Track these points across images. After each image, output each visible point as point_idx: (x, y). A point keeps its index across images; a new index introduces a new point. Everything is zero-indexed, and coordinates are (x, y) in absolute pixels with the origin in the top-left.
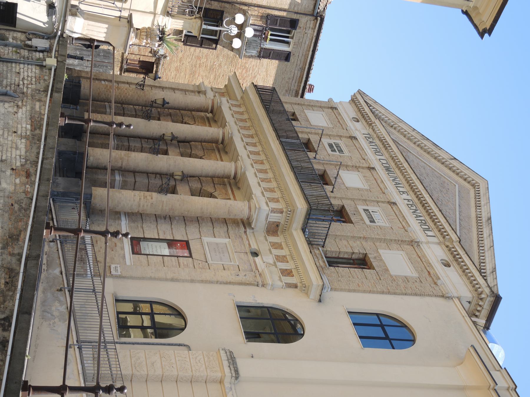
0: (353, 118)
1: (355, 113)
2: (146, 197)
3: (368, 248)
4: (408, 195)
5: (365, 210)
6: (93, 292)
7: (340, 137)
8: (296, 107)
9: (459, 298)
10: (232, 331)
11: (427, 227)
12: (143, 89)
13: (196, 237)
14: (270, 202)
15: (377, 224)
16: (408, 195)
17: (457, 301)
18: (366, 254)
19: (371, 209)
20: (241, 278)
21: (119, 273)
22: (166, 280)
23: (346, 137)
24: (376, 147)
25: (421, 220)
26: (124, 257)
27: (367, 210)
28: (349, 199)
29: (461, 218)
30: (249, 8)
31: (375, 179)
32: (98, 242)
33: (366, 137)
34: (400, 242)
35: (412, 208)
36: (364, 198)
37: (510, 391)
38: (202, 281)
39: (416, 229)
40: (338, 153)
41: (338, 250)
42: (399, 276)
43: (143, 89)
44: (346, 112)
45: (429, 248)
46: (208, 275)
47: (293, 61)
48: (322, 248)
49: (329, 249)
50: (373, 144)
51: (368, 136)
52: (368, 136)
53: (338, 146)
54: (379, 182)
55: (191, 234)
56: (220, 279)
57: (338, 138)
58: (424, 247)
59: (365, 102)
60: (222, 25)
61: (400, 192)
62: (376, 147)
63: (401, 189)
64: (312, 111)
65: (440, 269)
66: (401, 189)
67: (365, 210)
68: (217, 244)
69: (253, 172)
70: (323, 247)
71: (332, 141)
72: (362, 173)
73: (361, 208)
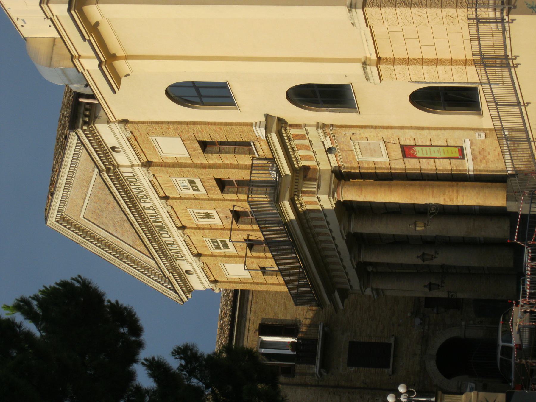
0: (192, 274)
1: (189, 279)
2: (450, 201)
3: (201, 158)
4: (144, 207)
5: (198, 190)
6: (484, 56)
7: (212, 256)
8: (262, 281)
9: (109, 122)
10: (362, 92)
11: (129, 180)
12: (449, 292)
13: (393, 161)
14: (316, 202)
15: (186, 179)
16: (144, 207)
17: (112, 119)
18: (204, 152)
19: (191, 192)
20: (350, 132)
21: (477, 133)
22: (429, 128)
23: (205, 255)
24: (171, 248)
25: (135, 185)
26: (471, 144)
27: (194, 190)
28: (215, 200)
29: (86, 189)
30: (317, 383)
31: (178, 218)
32: (497, 154)
33: (182, 257)
34: (163, 164)
35: (142, 195)
36: (196, 201)
37: (77, 55)
38: (392, 128)
39: (143, 177)
40: (218, 240)
41: (236, 155)
42: (172, 137)
43: (449, 292)
44: (200, 279)
45: (131, 161)
46: (385, 133)
47: (255, 324)
48: (254, 156)
49: (246, 155)
50: (173, 251)
51: (178, 258)
52: (178, 258)
53: (217, 247)
54: (174, 216)
55: (399, 164)
56: (372, 130)
57: (214, 254)
58: (136, 162)
59: (177, 293)
60: (351, 363)
61: (154, 209)
62: (171, 248)
63: (151, 211)
64: (241, 277)
65: (125, 145)
66: (151, 211)
67: (198, 190)
68: (372, 156)
69: (330, 226)
70: (253, 158)
71: (223, 250)
72: (193, 223)
73: (202, 191)
